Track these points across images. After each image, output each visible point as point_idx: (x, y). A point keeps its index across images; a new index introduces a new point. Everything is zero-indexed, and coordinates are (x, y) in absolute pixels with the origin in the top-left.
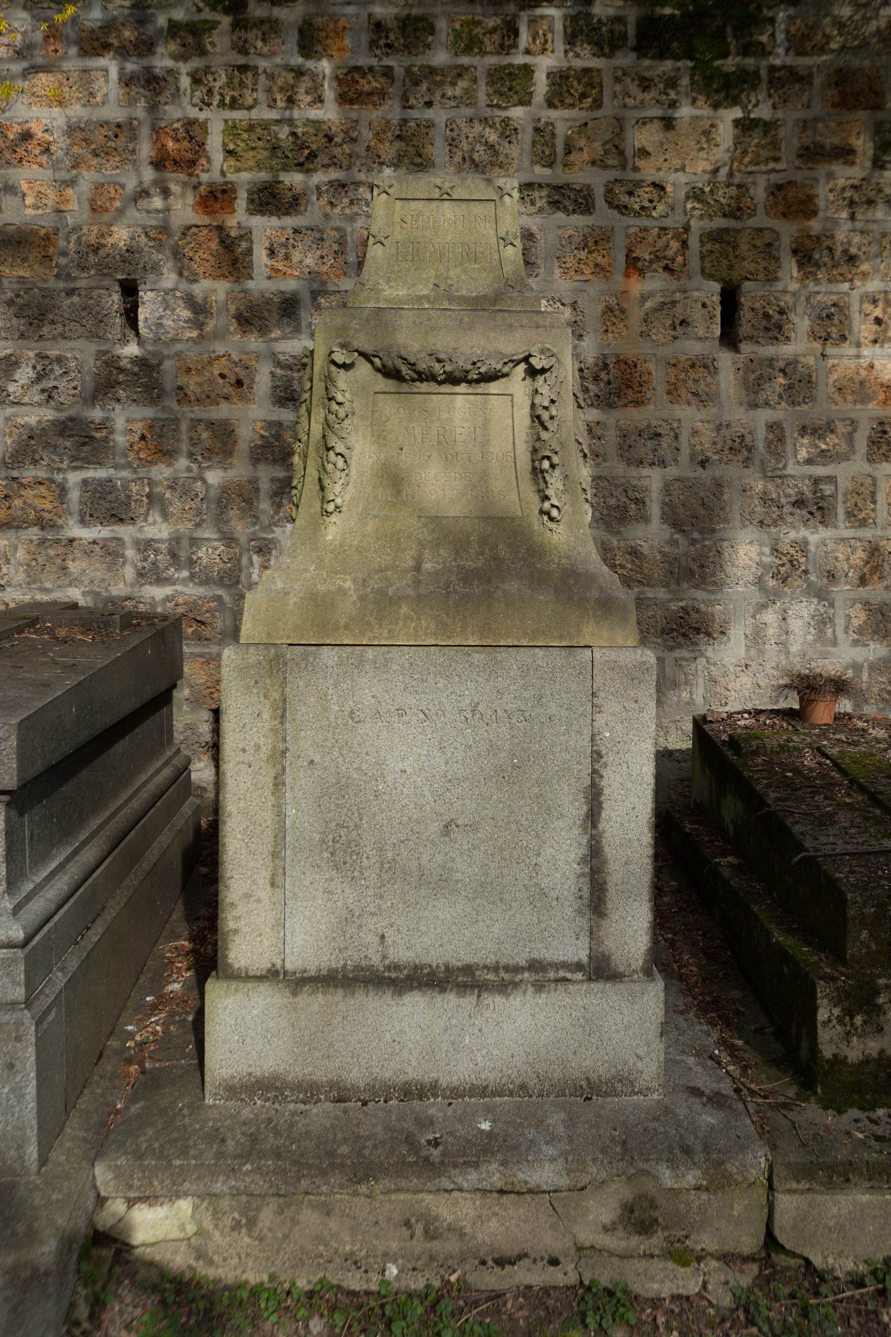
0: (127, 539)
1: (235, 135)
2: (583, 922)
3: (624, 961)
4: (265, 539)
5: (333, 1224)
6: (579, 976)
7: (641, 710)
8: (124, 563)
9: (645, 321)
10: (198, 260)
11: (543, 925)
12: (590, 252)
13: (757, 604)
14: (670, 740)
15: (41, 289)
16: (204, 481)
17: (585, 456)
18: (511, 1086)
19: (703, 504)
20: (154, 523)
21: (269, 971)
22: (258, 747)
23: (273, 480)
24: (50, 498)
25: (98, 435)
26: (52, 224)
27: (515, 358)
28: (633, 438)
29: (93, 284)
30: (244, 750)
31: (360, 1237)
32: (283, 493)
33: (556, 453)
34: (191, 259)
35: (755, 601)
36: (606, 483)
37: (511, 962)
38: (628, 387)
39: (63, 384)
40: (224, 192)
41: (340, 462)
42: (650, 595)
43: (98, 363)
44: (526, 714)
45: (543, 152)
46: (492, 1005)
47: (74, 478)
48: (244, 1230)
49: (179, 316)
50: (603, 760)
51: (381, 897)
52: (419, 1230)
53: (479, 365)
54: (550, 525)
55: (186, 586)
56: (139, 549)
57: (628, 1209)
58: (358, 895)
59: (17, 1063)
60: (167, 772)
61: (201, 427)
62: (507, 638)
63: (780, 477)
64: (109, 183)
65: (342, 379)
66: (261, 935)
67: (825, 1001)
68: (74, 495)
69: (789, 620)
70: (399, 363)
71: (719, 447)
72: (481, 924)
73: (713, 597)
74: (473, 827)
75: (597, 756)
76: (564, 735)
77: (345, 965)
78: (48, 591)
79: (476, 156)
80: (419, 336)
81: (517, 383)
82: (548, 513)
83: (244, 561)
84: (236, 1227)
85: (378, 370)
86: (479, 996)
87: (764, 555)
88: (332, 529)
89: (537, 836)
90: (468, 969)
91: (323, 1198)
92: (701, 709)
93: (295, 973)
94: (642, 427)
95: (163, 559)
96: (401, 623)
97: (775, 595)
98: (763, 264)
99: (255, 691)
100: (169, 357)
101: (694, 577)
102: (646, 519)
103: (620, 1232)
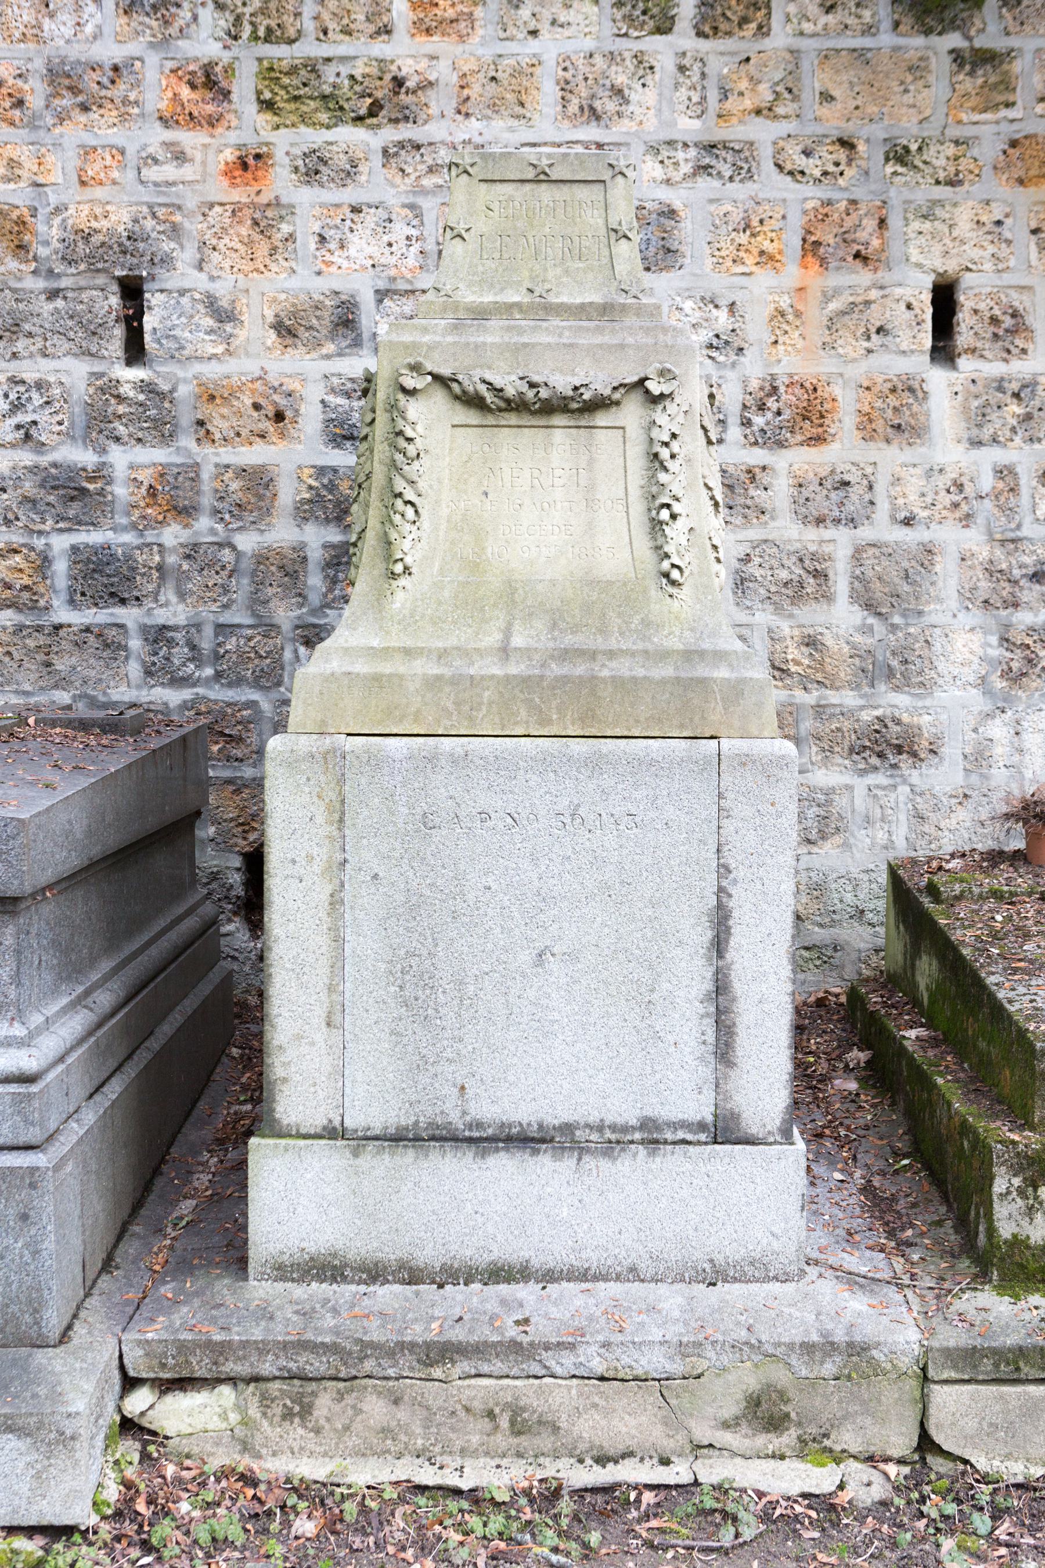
0: (131, 625)
1: (271, 79)
2: (706, 1072)
3: (757, 1120)
4: (315, 626)
5: (402, 1414)
6: (703, 1137)
7: (779, 815)
8: (127, 658)
9: (829, 328)
10: (224, 249)
11: (658, 1076)
12: (753, 235)
13: (980, 713)
14: (861, 896)
15: (14, 291)
16: (234, 548)
17: (716, 505)
18: (619, 1269)
19: (907, 577)
20: (166, 604)
21: (324, 1128)
22: (310, 858)
23: (326, 546)
24: (28, 571)
25: (91, 487)
26: (28, 203)
27: (626, 381)
28: (811, 488)
29: (83, 283)
30: (294, 862)
31: (434, 1430)
32: (338, 564)
33: (677, 500)
34: (214, 249)
35: (976, 709)
36: (775, 550)
37: (620, 1121)
38: (805, 418)
39: (43, 417)
40: (258, 156)
41: (410, 511)
42: (834, 701)
43: (91, 391)
44: (637, 819)
45: (690, 99)
46: (594, 1171)
47: (60, 543)
48: (297, 1420)
49: (198, 325)
50: (732, 876)
51: (461, 1040)
52: (504, 1422)
53: (582, 390)
54: (670, 589)
55: (211, 688)
56: (146, 639)
57: (754, 1402)
58: (433, 1037)
59: (32, 1213)
60: (191, 923)
61: (230, 474)
62: (616, 726)
63: (1013, 541)
64: (104, 147)
65: (414, 409)
66: (315, 1084)
67: (1003, 1169)
68: (61, 567)
69: (1024, 736)
70: (482, 389)
71: (929, 500)
72: (582, 1074)
73: (920, 704)
74: (572, 956)
75: (723, 870)
76: (684, 844)
77: (416, 1123)
78: (26, 693)
79: (597, 104)
80: (507, 355)
81: (631, 413)
82: (666, 575)
83: (288, 655)
84: (288, 1415)
85: (457, 398)
86: (579, 1159)
87: (990, 646)
88: (400, 595)
89: (651, 967)
90: (568, 1128)
91: (391, 1383)
92: (901, 850)
93: (356, 1131)
94: (823, 474)
95: (180, 652)
96: (484, 708)
97: (1005, 700)
98: (991, 249)
99: (307, 790)
100: (185, 381)
101: (894, 676)
102: (828, 598)
103: (745, 1429)
